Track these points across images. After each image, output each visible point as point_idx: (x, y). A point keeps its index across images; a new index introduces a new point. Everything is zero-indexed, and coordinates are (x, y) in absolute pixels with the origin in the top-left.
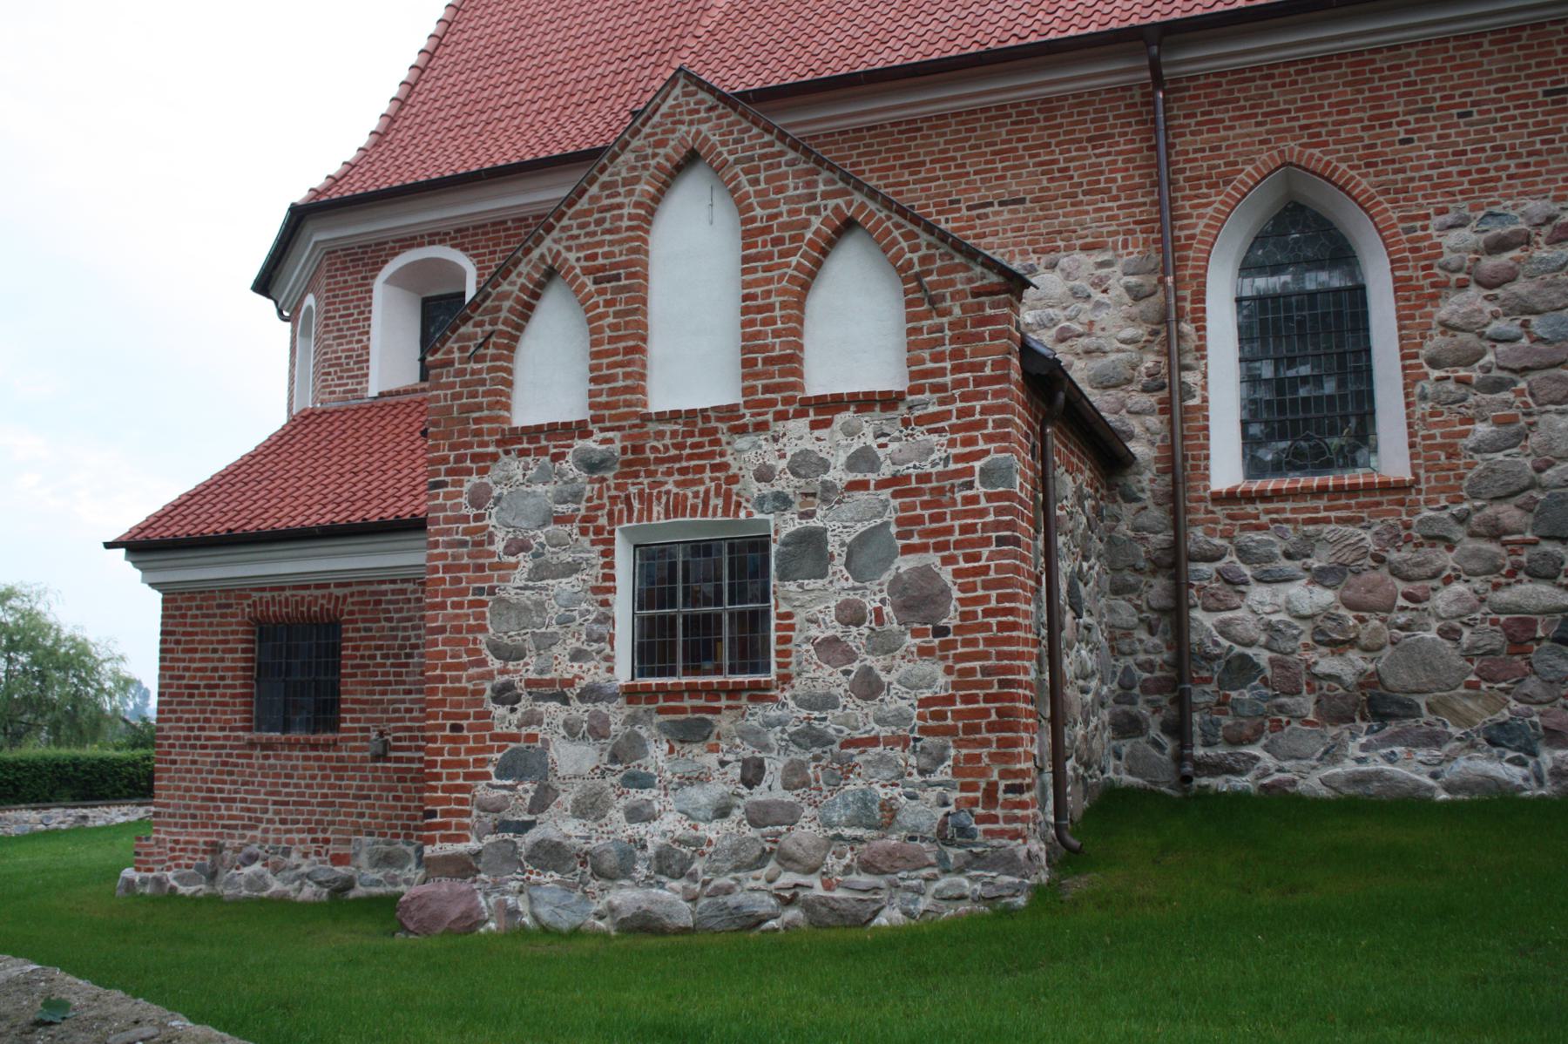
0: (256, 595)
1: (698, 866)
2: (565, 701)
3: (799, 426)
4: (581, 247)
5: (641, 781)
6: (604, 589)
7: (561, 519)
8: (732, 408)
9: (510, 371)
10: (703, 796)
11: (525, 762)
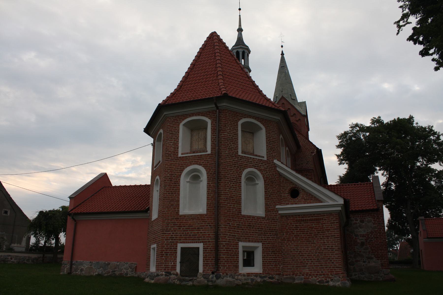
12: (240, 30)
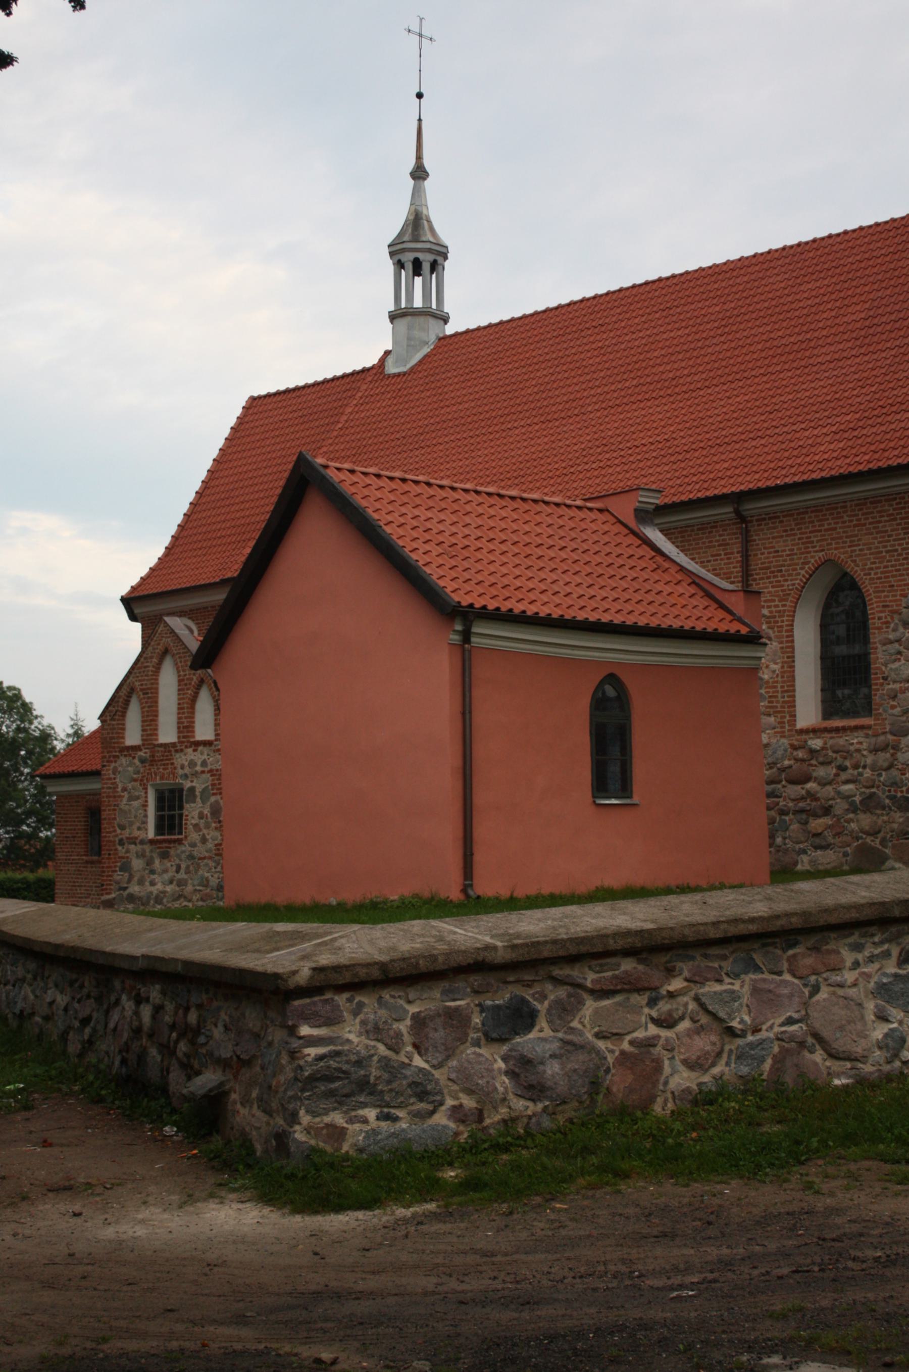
0: (88, 797)
1: (165, 900)
2: (135, 844)
3: (190, 750)
4: (140, 681)
5: (152, 872)
6: (145, 806)
7: (135, 780)
8: (174, 743)
9: (124, 724)
10: (166, 877)
11: (126, 867)
12: (419, 173)
